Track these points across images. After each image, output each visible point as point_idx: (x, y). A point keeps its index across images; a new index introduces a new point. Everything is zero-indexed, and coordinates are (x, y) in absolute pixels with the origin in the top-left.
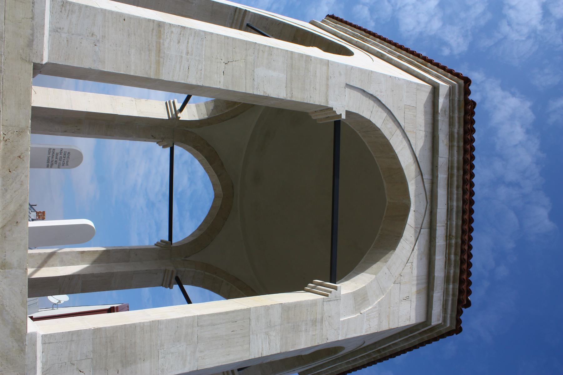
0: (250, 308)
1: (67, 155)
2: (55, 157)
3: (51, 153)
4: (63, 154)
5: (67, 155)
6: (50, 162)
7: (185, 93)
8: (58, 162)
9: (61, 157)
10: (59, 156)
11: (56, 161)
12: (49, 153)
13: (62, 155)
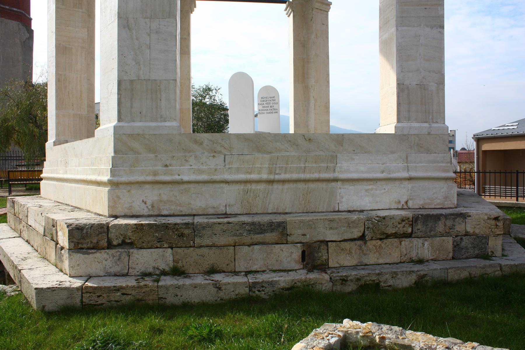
2: (267, 108)
8: (271, 105)
10: (265, 105)
13: (264, 103)
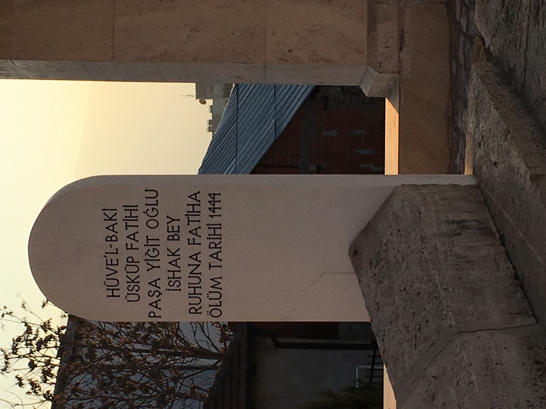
1: (121, 276)
2: (184, 261)
3: (206, 286)
5: (121, 276)
6: (204, 232)
7: (373, 307)
8: (161, 233)
9: (152, 262)
10: (162, 273)
12: (216, 282)
13: (145, 277)
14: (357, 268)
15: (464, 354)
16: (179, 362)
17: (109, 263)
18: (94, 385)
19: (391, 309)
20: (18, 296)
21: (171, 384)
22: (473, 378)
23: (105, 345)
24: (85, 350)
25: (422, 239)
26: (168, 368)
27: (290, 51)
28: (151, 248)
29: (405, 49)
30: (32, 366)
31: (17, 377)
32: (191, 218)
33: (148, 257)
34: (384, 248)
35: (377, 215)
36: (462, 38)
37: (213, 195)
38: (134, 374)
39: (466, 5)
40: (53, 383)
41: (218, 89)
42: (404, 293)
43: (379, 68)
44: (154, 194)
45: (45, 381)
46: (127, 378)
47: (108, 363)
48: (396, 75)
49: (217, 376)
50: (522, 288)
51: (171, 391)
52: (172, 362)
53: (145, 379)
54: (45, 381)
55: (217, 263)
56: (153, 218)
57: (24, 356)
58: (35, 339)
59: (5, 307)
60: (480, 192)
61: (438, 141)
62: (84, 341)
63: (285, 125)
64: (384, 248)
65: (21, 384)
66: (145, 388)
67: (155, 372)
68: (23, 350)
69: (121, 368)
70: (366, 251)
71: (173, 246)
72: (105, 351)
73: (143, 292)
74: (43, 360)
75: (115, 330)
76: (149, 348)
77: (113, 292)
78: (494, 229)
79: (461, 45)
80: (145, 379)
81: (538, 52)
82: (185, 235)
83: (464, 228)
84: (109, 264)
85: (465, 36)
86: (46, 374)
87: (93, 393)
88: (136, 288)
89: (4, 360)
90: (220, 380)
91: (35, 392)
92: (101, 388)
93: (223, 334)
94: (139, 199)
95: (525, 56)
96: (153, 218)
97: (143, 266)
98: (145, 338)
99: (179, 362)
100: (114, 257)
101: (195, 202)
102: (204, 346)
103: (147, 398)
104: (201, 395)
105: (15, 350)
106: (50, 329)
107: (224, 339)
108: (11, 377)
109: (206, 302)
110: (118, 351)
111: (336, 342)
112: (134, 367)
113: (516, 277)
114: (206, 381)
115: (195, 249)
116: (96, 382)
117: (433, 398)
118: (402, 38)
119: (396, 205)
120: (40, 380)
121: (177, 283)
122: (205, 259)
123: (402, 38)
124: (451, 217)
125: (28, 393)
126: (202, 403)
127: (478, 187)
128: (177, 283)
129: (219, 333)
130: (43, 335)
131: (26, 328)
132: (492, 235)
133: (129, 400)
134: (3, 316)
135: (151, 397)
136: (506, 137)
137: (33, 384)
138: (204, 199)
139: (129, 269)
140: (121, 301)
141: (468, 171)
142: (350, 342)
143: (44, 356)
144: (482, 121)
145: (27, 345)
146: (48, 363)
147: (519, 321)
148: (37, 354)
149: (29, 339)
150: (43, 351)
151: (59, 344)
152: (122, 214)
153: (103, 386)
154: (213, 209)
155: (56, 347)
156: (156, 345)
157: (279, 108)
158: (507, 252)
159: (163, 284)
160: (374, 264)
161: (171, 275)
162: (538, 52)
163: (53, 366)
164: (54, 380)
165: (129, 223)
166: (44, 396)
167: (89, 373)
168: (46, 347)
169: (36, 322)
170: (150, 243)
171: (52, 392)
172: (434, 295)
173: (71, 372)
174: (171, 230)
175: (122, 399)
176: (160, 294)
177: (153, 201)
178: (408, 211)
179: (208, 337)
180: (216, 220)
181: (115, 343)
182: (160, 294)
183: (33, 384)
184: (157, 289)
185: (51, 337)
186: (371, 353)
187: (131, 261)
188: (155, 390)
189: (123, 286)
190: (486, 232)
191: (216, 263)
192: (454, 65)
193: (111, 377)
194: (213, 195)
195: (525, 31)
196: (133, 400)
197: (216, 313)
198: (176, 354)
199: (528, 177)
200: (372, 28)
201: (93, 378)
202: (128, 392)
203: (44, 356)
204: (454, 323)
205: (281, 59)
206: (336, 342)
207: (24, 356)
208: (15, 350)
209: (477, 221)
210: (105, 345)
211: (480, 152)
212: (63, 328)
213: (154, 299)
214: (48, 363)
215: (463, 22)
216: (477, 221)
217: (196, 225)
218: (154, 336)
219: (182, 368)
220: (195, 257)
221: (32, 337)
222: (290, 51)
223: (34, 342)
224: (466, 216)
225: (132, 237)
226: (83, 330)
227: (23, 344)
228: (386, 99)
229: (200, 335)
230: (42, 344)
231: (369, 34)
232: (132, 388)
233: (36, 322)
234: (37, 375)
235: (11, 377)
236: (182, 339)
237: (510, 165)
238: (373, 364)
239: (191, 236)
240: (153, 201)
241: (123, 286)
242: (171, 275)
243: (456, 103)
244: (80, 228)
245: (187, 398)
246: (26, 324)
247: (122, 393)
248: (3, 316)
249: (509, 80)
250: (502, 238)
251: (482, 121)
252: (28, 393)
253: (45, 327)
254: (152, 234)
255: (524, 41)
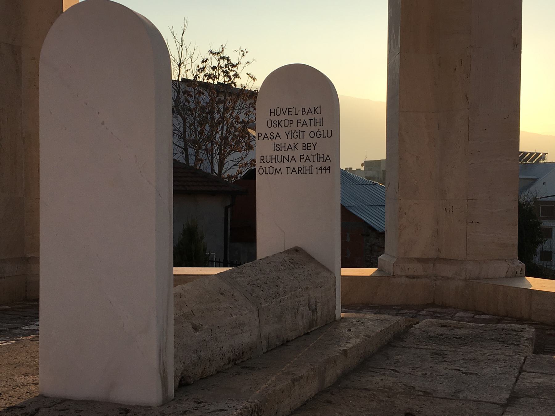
0: (177, 167)
1: (282, 117)
2: (290, 153)
3: (277, 166)
4: (275, 130)
5: (282, 117)
6: (308, 165)
7: (267, 260)
8: (307, 139)
10: (284, 140)
11: (306, 147)
12: (278, 171)
13: (282, 131)
14: (288, 252)
15: (247, 311)
16: (216, 151)
17: (290, 110)
18: (203, 103)
19: (268, 270)
20: (254, 59)
21: (204, 148)
22: (234, 317)
23: (226, 109)
24: (223, 98)
25: (307, 288)
26: (212, 145)
27: (405, 213)
28: (298, 134)
29: (407, 279)
30: (214, 68)
31: (207, 59)
32: (316, 157)
33: (293, 132)
34: (301, 266)
35: (318, 263)
36: (415, 312)
37: (329, 168)
38: (210, 126)
39: (434, 314)
40: (204, 80)
41: (370, 174)
42: (277, 278)
43: (397, 264)
44: (329, 135)
45: (205, 75)
46: (207, 122)
47: (216, 111)
48: (392, 274)
49: (209, 173)
50: (282, 345)
51: (200, 148)
52: (216, 148)
53: (206, 133)
54: (205, 75)
55: (290, 172)
56: (315, 134)
57: (219, 63)
58: (229, 69)
59: (247, 52)
60: (332, 322)
61: (360, 299)
62: (228, 97)
63: (353, 212)
64: (301, 266)
65: (203, 62)
66: (201, 133)
67: (210, 139)
68: (223, 63)
69: (213, 118)
70: (297, 256)
71: (300, 146)
72: (222, 110)
73: (273, 130)
74: (217, 74)
75: (234, 115)
76: (224, 135)
77: (273, 112)
78: (313, 329)
79: (411, 311)
80: (206, 133)
81: (415, 354)
82: (306, 153)
83: (313, 312)
84: (289, 110)
85: (416, 313)
86: (209, 76)
87: (198, 103)
88: (275, 126)
89: (217, 52)
90: (206, 176)
91: (199, 70)
92: (201, 107)
93: (232, 177)
94: (325, 127)
95: (411, 347)
96: (315, 134)
97: (288, 130)
98: (230, 132)
99: (216, 151)
100: (293, 113)
101: (325, 158)
102: (225, 166)
103: (196, 134)
104: (197, 164)
105: (223, 58)
106: (235, 78)
107: (230, 177)
108: (208, 56)
109: (267, 165)
110: (222, 117)
111: (229, 240)
112: (212, 127)
113: (286, 343)
114: (205, 167)
115: (298, 158)
116: (205, 105)
117: (222, 294)
118: (414, 277)
119: (325, 274)
120: (206, 73)
121: (278, 149)
122: (293, 165)
123: (414, 277)
124: (319, 305)
125: (198, 66)
126: (193, 165)
127: (335, 320)
128: (278, 149)
129: (233, 175)
130: (231, 74)
131: (235, 64)
132: (310, 328)
133: (194, 123)
134: (242, 51)
135: (196, 135)
136: (366, 336)
137: (203, 69)
138: (327, 164)
139: (286, 121)
140: (269, 118)
141: (343, 315)
142: (228, 249)
143: (219, 74)
144: (372, 324)
145: (226, 65)
146: (215, 77)
147: (265, 343)
148: (221, 70)
149: (229, 66)
150: (222, 74)
151: (226, 83)
152: (318, 117)
153: (203, 109)
154: (321, 169)
155: (225, 82)
156: (226, 138)
157: (363, 208)
158: (300, 336)
159: (278, 141)
160: (292, 261)
161: (283, 145)
162: (415, 354)
163: (214, 80)
164: (205, 81)
165: (312, 121)
166: (197, 75)
167: (210, 100)
168: (224, 76)
169: (239, 69)
170: (301, 133)
171: (198, 80)
172: (277, 295)
173: (210, 90)
174: (309, 145)
175: (195, 119)
176: (272, 139)
177: (325, 135)
178: (321, 281)
179: (230, 168)
180: (315, 171)
181: (227, 115)
182: (272, 139)
183: (203, 69)
184: (275, 137)
185: (231, 79)
186: (222, 261)
187: (291, 122)
188: (200, 138)
189: (276, 118)
190: (311, 324)
191: (290, 171)
192: (399, 307)
193: (207, 113)
194: (329, 168)
195: (426, 347)
196: (194, 126)
197: (261, 171)
198: (221, 149)
199: (346, 348)
200: (419, 260)
201: (207, 103)
202: (199, 122)
203: (219, 74)
204: (263, 306)
205: (400, 208)
206: (229, 240)
207: (219, 63)
208: (223, 58)
209: (317, 320)
210: (226, 109)
211: (355, 322)
212: (235, 85)
213: (269, 136)
214: (215, 77)
215: (424, 313)
216: (317, 320)
217: (312, 159)
218: (231, 137)
219: (212, 154)
220: (293, 159)
221: (230, 67)
222: (405, 213)
223: (227, 69)
224: (319, 314)
225: (305, 123)
226: (234, 97)
227: (226, 62)
228: (374, 270)
229: (231, 164)
230: (226, 73)
231: (415, 258)
232: (201, 125)
233: (239, 69)
234: (208, 71)
235: (208, 56)
236: (229, 154)
237: (350, 338)
238: (216, 262)
239: (305, 157)
240: (325, 135)
241: (276, 118)
242: (283, 145)
243: (379, 308)
244: (306, 92)
245: (196, 156)
246: (237, 64)
247: (198, 119)
248: (242, 51)
249: (395, 339)
250: (308, 334)
251: (372, 324)
252: (198, 66)
253: (236, 75)
254: (306, 135)
255: (420, 347)
